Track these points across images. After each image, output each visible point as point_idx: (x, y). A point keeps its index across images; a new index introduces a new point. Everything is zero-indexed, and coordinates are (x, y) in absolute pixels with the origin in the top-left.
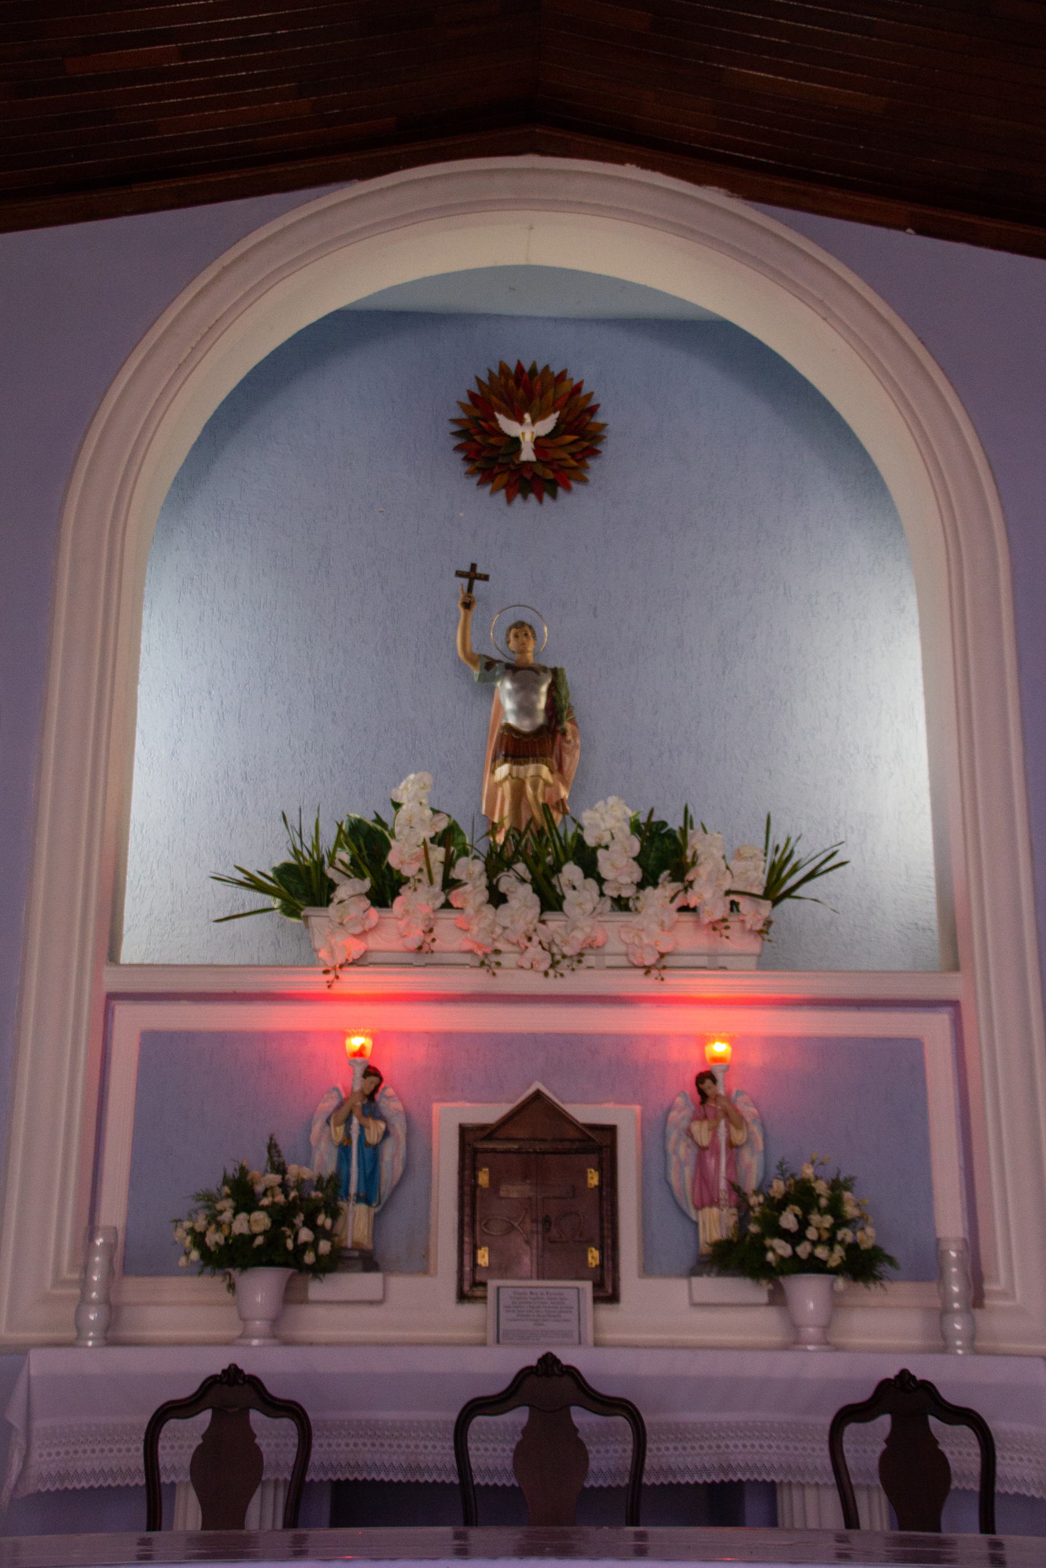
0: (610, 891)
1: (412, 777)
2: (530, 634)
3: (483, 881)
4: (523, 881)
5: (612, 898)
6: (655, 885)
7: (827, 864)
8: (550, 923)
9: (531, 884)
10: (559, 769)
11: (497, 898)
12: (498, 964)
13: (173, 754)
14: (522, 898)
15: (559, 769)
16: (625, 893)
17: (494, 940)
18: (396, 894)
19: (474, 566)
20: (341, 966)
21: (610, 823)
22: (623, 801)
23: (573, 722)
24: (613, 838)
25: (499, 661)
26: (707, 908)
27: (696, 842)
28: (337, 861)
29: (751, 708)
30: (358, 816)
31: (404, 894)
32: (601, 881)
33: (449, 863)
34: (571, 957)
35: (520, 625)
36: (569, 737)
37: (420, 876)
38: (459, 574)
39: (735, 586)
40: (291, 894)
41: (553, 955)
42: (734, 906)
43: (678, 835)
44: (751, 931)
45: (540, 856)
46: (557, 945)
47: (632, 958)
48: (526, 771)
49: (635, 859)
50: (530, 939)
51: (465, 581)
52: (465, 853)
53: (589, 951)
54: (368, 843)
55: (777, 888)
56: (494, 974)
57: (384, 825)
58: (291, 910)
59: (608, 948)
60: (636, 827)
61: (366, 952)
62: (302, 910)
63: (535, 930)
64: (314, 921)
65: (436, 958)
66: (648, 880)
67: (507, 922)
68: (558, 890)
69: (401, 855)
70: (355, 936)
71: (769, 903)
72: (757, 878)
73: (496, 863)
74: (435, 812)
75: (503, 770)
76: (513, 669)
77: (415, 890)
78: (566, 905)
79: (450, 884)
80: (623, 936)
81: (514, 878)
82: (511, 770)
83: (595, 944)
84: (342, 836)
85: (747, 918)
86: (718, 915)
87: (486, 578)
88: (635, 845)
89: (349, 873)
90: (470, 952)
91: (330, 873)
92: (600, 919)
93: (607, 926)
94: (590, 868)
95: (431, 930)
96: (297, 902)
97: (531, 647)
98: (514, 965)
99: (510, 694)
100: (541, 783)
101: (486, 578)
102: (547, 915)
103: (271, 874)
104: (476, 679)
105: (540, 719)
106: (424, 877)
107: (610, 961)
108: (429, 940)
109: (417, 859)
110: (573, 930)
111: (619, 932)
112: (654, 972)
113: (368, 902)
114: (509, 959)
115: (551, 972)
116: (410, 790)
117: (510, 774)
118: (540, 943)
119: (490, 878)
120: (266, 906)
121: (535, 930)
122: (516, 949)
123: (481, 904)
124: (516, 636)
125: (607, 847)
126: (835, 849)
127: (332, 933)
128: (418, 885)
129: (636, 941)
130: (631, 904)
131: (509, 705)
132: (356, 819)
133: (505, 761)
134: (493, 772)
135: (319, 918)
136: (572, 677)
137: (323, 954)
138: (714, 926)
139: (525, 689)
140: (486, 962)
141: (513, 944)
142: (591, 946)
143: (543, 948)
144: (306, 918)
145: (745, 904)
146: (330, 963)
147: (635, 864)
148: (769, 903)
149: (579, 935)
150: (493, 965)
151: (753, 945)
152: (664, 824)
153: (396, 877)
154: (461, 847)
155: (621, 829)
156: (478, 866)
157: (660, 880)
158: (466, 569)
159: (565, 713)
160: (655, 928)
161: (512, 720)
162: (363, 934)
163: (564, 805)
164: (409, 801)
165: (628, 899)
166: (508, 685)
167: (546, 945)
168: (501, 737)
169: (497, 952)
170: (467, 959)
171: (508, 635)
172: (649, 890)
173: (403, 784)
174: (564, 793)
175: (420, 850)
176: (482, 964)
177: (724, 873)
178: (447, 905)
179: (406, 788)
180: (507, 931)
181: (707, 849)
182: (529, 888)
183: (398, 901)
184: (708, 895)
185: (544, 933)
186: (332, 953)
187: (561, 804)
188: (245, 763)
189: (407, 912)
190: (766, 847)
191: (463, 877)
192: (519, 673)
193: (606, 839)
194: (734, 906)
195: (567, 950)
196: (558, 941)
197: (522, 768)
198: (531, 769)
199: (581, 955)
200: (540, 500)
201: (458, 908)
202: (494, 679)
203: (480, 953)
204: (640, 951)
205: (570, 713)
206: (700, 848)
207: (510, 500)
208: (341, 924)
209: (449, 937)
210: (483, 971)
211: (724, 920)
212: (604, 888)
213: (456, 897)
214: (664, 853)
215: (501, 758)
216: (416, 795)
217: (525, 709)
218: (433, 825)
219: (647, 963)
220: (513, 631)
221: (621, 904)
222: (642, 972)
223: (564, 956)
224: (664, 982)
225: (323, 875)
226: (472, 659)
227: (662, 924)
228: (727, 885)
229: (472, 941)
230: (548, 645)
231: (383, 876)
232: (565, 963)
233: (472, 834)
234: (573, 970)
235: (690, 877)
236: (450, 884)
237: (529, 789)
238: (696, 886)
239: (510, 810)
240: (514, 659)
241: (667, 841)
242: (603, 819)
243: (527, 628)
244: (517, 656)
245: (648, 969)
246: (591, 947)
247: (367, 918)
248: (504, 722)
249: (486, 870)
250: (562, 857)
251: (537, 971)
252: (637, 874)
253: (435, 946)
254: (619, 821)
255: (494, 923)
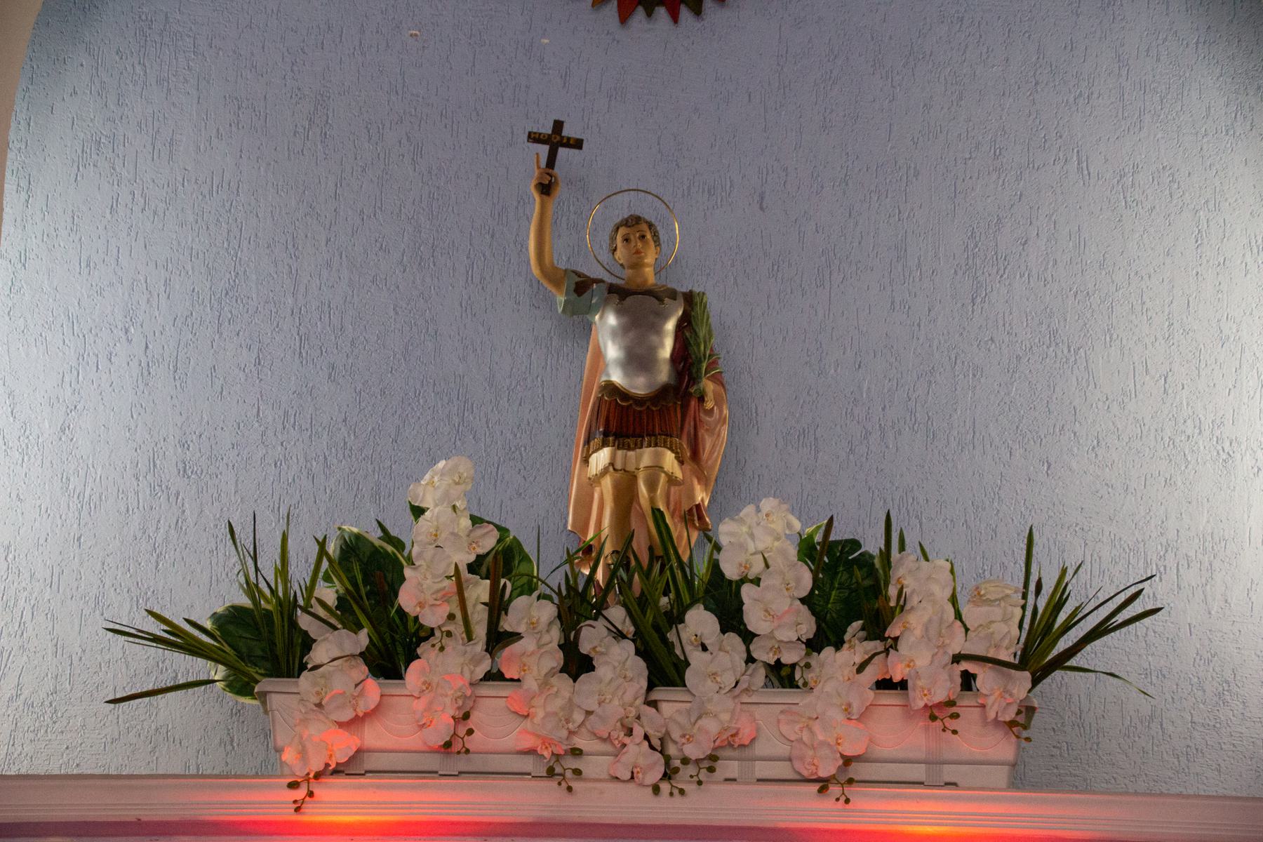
0: (764, 654)
1: (441, 464)
2: (649, 236)
3: (555, 634)
4: (620, 635)
5: (767, 665)
6: (838, 645)
7: (1125, 613)
8: (664, 707)
9: (633, 641)
10: (693, 456)
11: (577, 664)
12: (577, 772)
13: (63, 431)
14: (619, 665)
15: (693, 456)
16: (787, 658)
17: (571, 733)
18: (412, 656)
19: (558, 125)
20: (318, 776)
21: (764, 541)
22: (785, 507)
23: (717, 379)
24: (767, 566)
25: (601, 281)
26: (920, 683)
27: (908, 574)
28: (313, 601)
29: (1019, 358)
30: (355, 530)
31: (424, 657)
32: (748, 637)
33: (498, 606)
34: (698, 761)
35: (633, 222)
36: (709, 404)
37: (451, 628)
38: (534, 138)
39: (996, 157)
40: (241, 656)
41: (668, 759)
42: (968, 681)
43: (877, 562)
44: (997, 723)
45: (652, 598)
46: (675, 742)
47: (798, 765)
48: (638, 459)
49: (803, 601)
50: (630, 732)
51: (544, 150)
52: (529, 589)
53: (728, 753)
54: (369, 572)
55: (1045, 648)
56: (570, 789)
57: (398, 544)
58: (241, 685)
59: (760, 749)
60: (808, 550)
61: (359, 751)
62: (257, 682)
63: (638, 718)
64: (275, 701)
65: (476, 763)
66: (826, 636)
67: (592, 704)
68: (678, 651)
69: (420, 594)
70: (341, 725)
71: (1026, 675)
72: (1003, 631)
73: (576, 607)
74: (476, 521)
75: (601, 458)
76: (620, 294)
77: (442, 649)
78: (689, 675)
79: (498, 639)
80: (785, 729)
81: (605, 632)
82: (613, 457)
83: (737, 741)
84: (325, 564)
85: (990, 701)
86: (940, 695)
87: (578, 144)
88: (805, 580)
89: (333, 621)
90: (531, 752)
91: (304, 621)
92: (746, 699)
93: (759, 712)
94: (731, 618)
95: (466, 716)
96: (252, 670)
97: (650, 259)
98: (605, 776)
99: (614, 334)
100: (663, 478)
101: (578, 144)
102: (659, 694)
103: (208, 625)
104: (560, 310)
105: (663, 375)
106: (457, 628)
107: (762, 770)
108: (462, 731)
109: (446, 599)
110: (700, 717)
111: (779, 721)
112: (835, 790)
113: (365, 668)
114: (595, 766)
115: (665, 787)
116: (440, 488)
117: (612, 464)
118: (646, 737)
119: (565, 631)
120: (203, 677)
121: (638, 718)
122: (606, 747)
123: (551, 673)
124: (626, 240)
125: (757, 581)
126: (1140, 586)
127: (305, 721)
128: (446, 641)
129: (806, 737)
130: (797, 676)
131: (612, 351)
132: (351, 533)
133: (604, 444)
134: (586, 461)
135: (287, 697)
136: (717, 306)
137: (289, 756)
138: (933, 713)
139: (639, 328)
140: (558, 770)
141: (604, 740)
142: (731, 744)
143: (652, 747)
144: (263, 696)
145: (986, 678)
146: (300, 772)
147: (804, 609)
148: (1026, 675)
149: (712, 726)
150: (569, 774)
151: (1004, 748)
152: (855, 544)
153: (412, 628)
154: (525, 579)
155: (783, 552)
156: (547, 611)
157: (847, 637)
158: (547, 129)
159: (704, 365)
160: (837, 715)
161: (616, 377)
162: (356, 722)
163: (701, 518)
164: (436, 505)
165: (793, 666)
166: (612, 320)
167: (656, 743)
168: (600, 400)
169: (576, 752)
170: (527, 764)
171: (613, 239)
172: (828, 652)
173: (427, 477)
174: (701, 496)
175: (450, 585)
176: (551, 773)
177: (950, 626)
178: (494, 676)
179: (431, 483)
180: (592, 717)
181: (920, 585)
182: (629, 647)
183: (415, 665)
184: (923, 660)
185: (652, 722)
186: (303, 754)
187: (694, 516)
188: (184, 445)
189: (428, 685)
190: (1026, 585)
191: (521, 629)
192: (629, 300)
193: (757, 567)
194: (968, 681)
195: (692, 751)
196: (676, 734)
197: (631, 453)
198: (646, 456)
199: (713, 758)
200: (675, 18)
201: (512, 680)
202: (591, 310)
203: (547, 754)
204: (811, 753)
205: (713, 365)
206: (910, 584)
207: (624, 18)
208: (319, 705)
209: (499, 727)
210: (553, 784)
211: (951, 703)
212: (752, 647)
213: (509, 659)
214: (851, 592)
215: (598, 439)
216: (446, 495)
217: (638, 359)
218: (472, 543)
219: (823, 773)
220: (622, 231)
221: (782, 676)
222: (815, 788)
223: (685, 761)
224: (850, 806)
225: (293, 624)
226: (554, 276)
227: (848, 709)
228: (958, 644)
229: (539, 736)
230: (686, 251)
231: (392, 628)
232: (691, 770)
233: (549, 566)
234: (700, 783)
235: (893, 631)
236: (498, 639)
237: (643, 489)
238: (902, 645)
239: (611, 521)
240: (622, 277)
241: (858, 574)
242: (752, 536)
243: (644, 227)
244: (628, 273)
245: (824, 785)
246: (731, 745)
247: (361, 694)
248: (604, 378)
249: (559, 616)
250: (686, 598)
251: (642, 785)
252: (808, 627)
253: (472, 743)
254: (778, 539)
255: (571, 705)
